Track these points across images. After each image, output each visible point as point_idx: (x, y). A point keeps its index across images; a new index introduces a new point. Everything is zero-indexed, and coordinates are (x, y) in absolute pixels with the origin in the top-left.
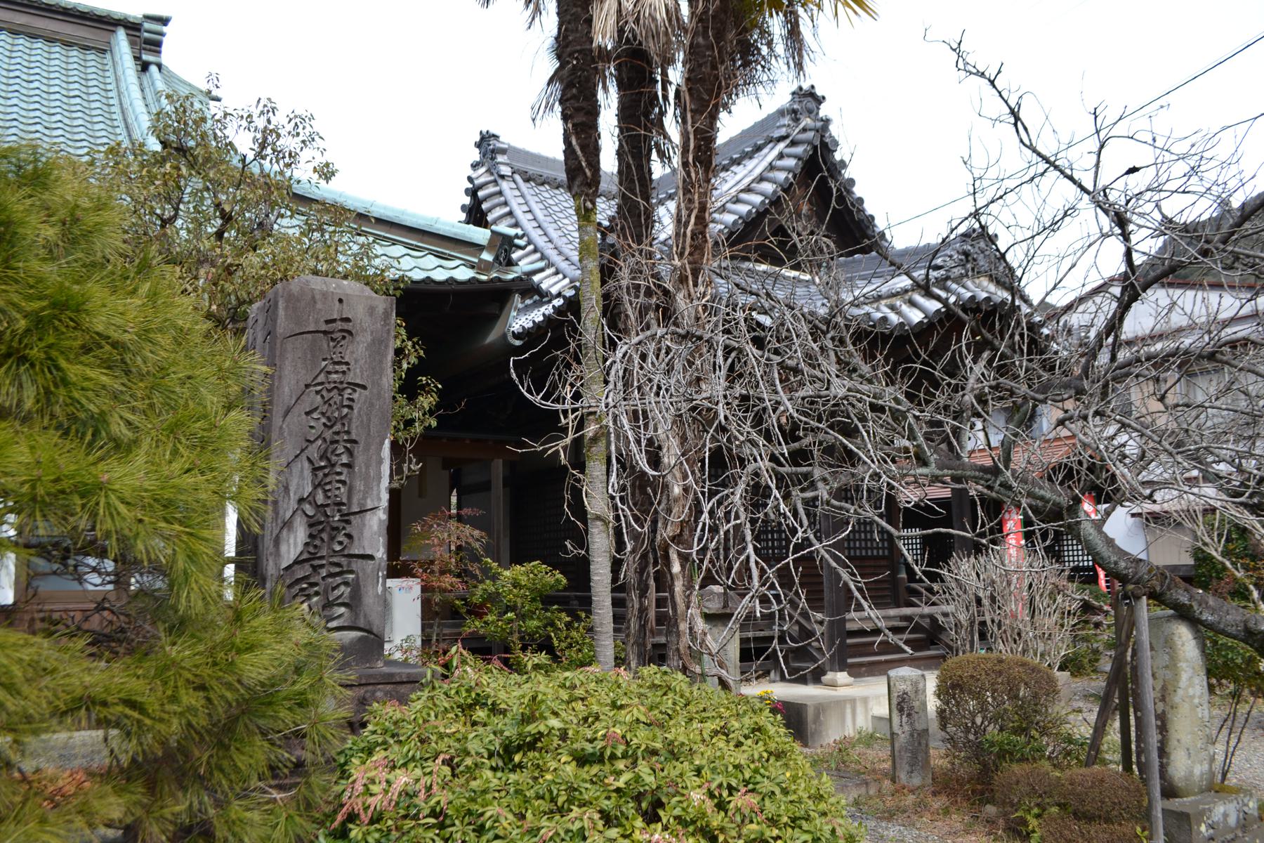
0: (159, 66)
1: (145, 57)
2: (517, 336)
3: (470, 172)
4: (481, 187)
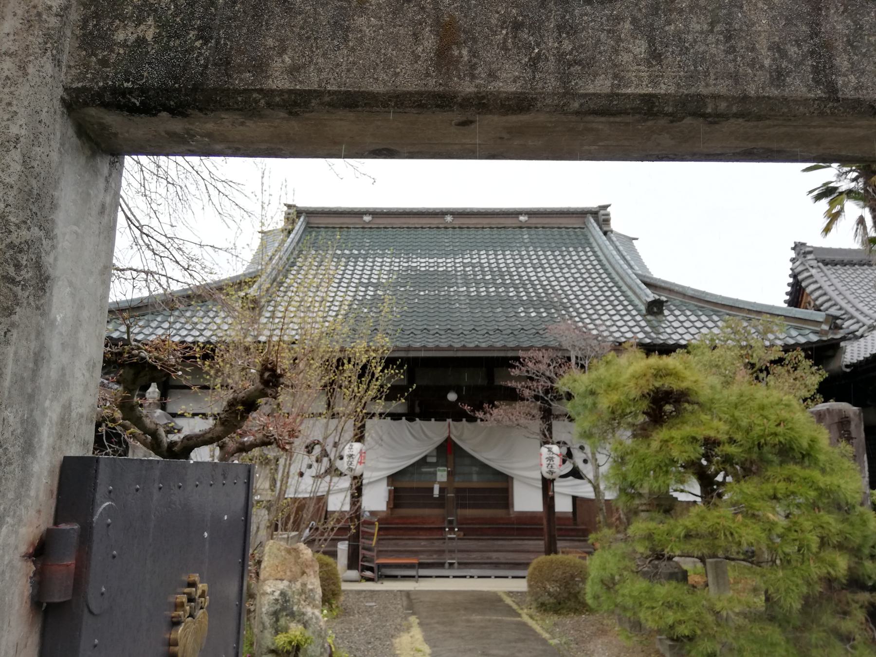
0: (612, 231)
1: (605, 229)
2: (847, 366)
3: (790, 265)
4: (799, 273)
